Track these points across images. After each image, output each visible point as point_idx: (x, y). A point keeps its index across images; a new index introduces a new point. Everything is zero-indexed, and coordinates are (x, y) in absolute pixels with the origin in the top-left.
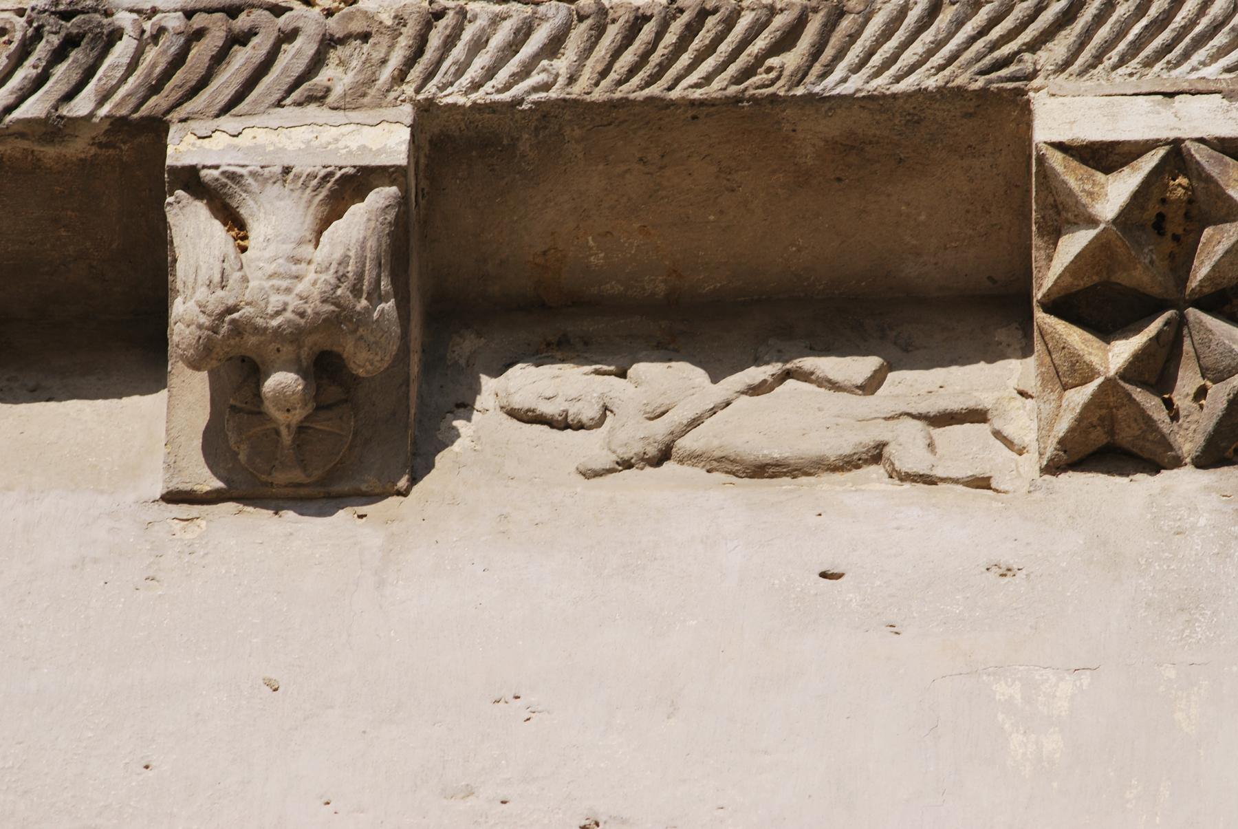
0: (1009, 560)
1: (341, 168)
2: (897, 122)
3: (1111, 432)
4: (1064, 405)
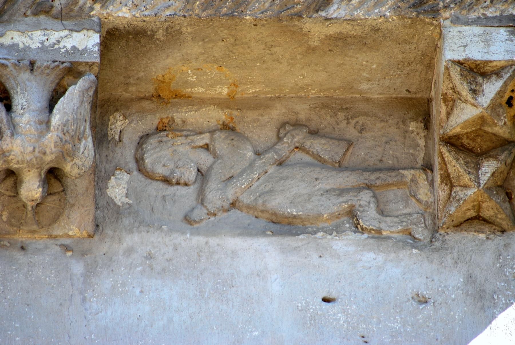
0: (427, 293)
1: (63, 63)
2: (366, 29)
3: (479, 211)
4: (453, 195)
